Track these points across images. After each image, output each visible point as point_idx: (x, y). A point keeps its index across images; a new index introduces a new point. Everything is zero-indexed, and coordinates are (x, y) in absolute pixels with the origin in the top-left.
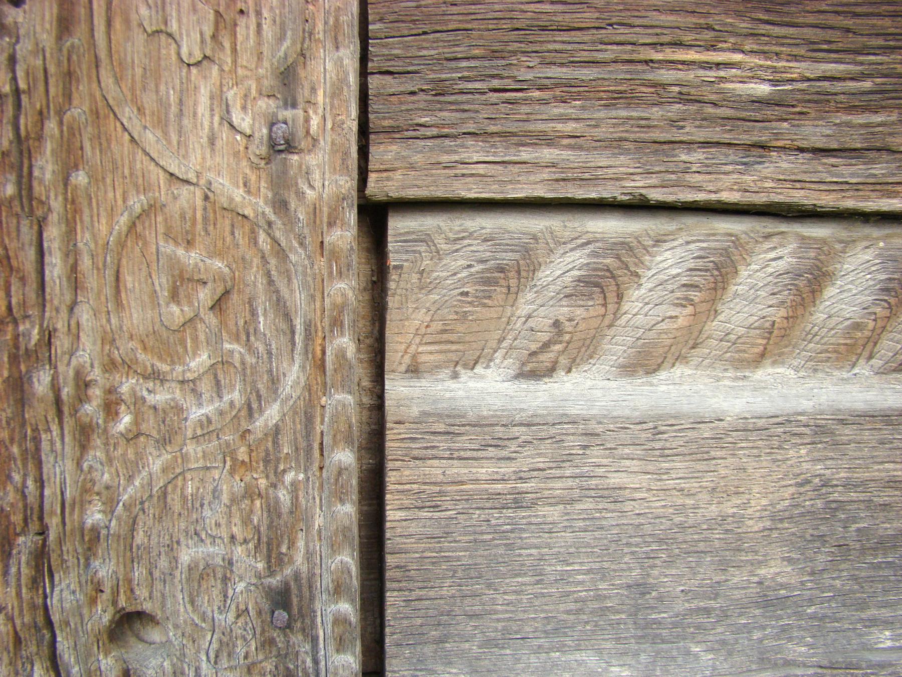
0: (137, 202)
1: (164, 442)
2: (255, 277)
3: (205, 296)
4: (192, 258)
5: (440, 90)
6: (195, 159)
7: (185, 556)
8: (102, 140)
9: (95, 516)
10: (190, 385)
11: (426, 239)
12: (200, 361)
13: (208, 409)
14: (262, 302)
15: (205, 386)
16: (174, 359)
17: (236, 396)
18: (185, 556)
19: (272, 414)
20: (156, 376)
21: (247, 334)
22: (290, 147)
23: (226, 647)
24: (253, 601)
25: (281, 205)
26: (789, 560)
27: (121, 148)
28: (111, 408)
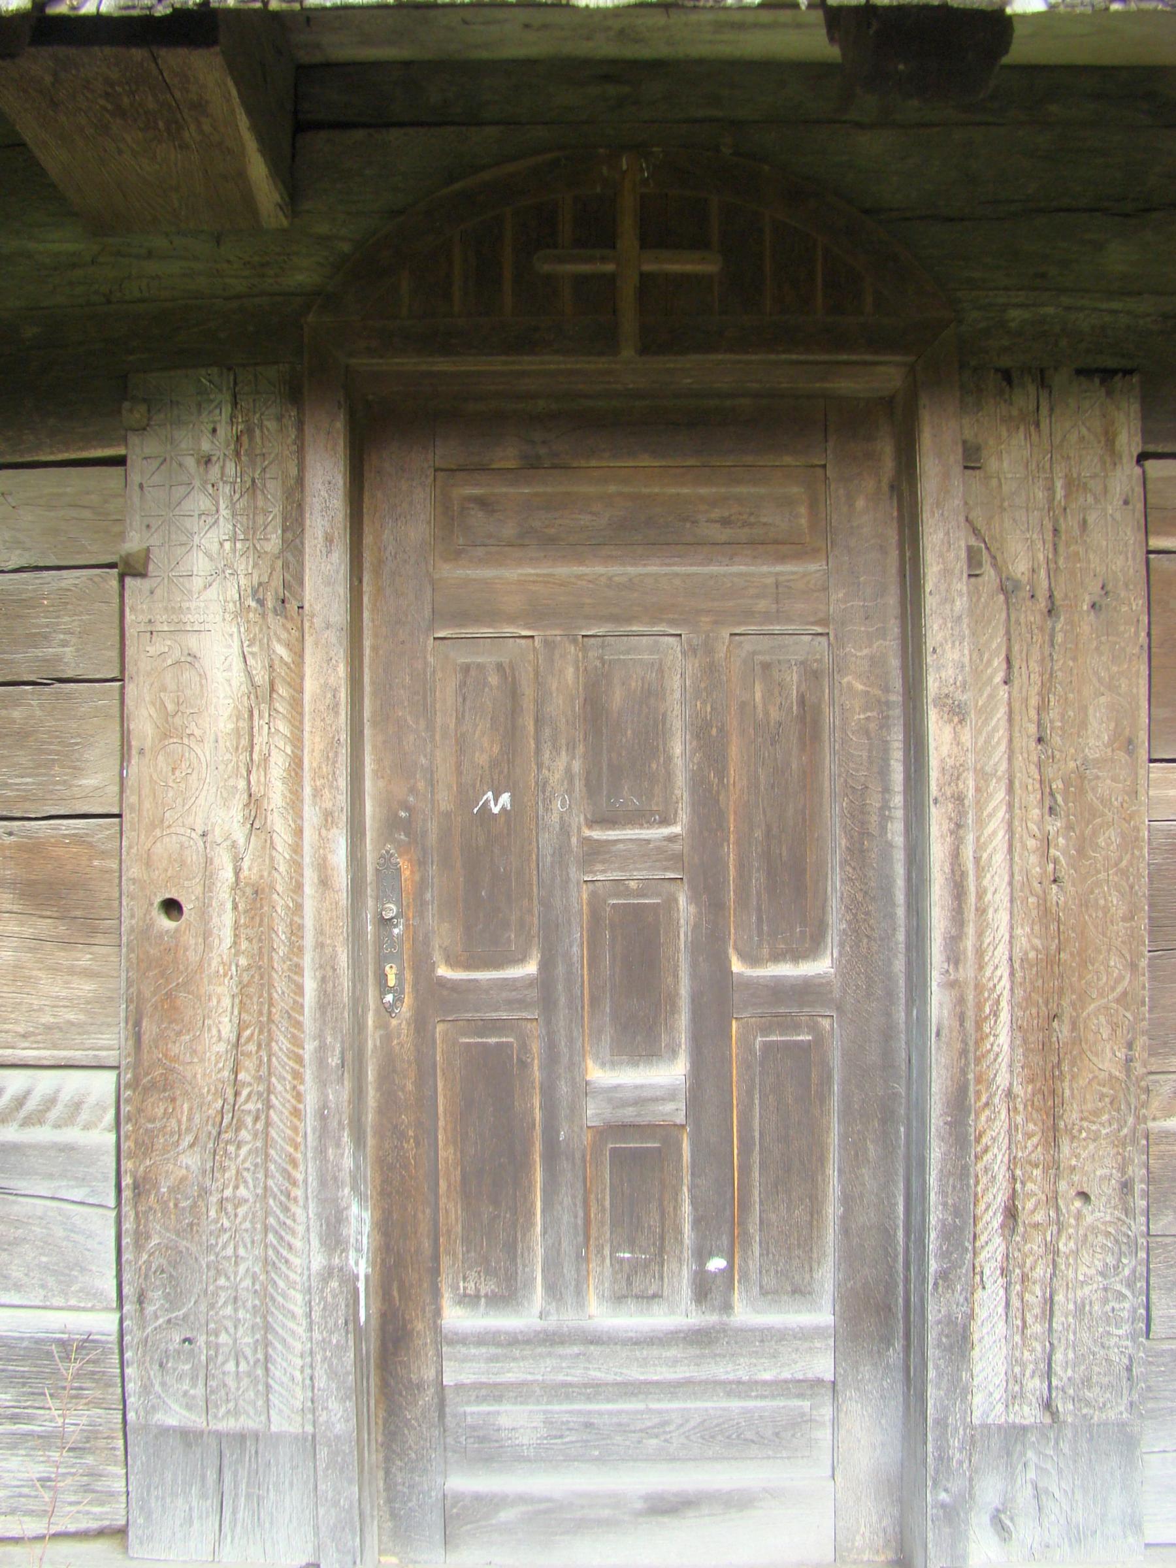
0: (1090, 1076)
1: (1094, 1140)
2: (1121, 1095)
3: (1107, 1100)
4: (1105, 1090)
5: (1165, 1043)
6: (1106, 1064)
7: (1098, 1173)
8: (1082, 1061)
9: (1073, 1162)
10: (1102, 1124)
11: (1157, 1082)
12: (1105, 1117)
13: (1108, 1130)
14: (1123, 1102)
15: (1107, 1124)
16: (1098, 1117)
17: (1115, 1126)
18: (1098, 1173)
19: (1125, 1131)
20: (1094, 1123)
21: (1118, 1110)
22: (1131, 1061)
23: (1109, 1201)
24: (1117, 1186)
25: (1128, 1076)
26: (958, 1514)
27: (1086, 1062)
28: (1080, 1132)
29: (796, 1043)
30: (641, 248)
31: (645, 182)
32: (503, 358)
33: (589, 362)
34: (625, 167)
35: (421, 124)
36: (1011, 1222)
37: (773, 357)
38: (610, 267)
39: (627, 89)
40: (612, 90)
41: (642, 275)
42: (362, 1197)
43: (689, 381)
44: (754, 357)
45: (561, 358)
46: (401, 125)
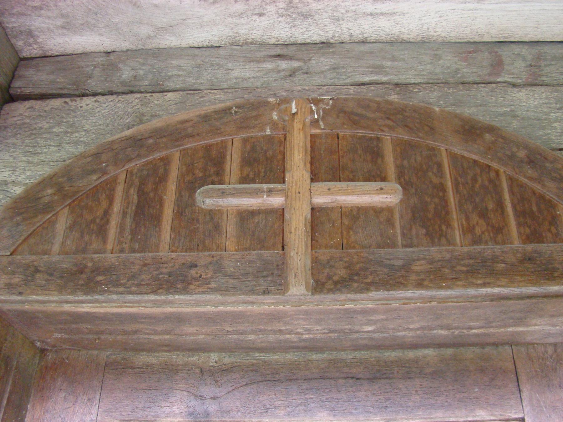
29: (205, 313)
30: (312, 180)
31: (315, 123)
32: (152, 297)
33: (252, 303)
34: (294, 110)
35: (111, 93)
36: (138, 333)
37: (472, 291)
38: (277, 201)
39: (296, 64)
40: (284, 64)
41: (311, 135)
42: (458, 333)
43: (370, 328)
44: (449, 293)
45: (219, 297)
46: (94, 95)
